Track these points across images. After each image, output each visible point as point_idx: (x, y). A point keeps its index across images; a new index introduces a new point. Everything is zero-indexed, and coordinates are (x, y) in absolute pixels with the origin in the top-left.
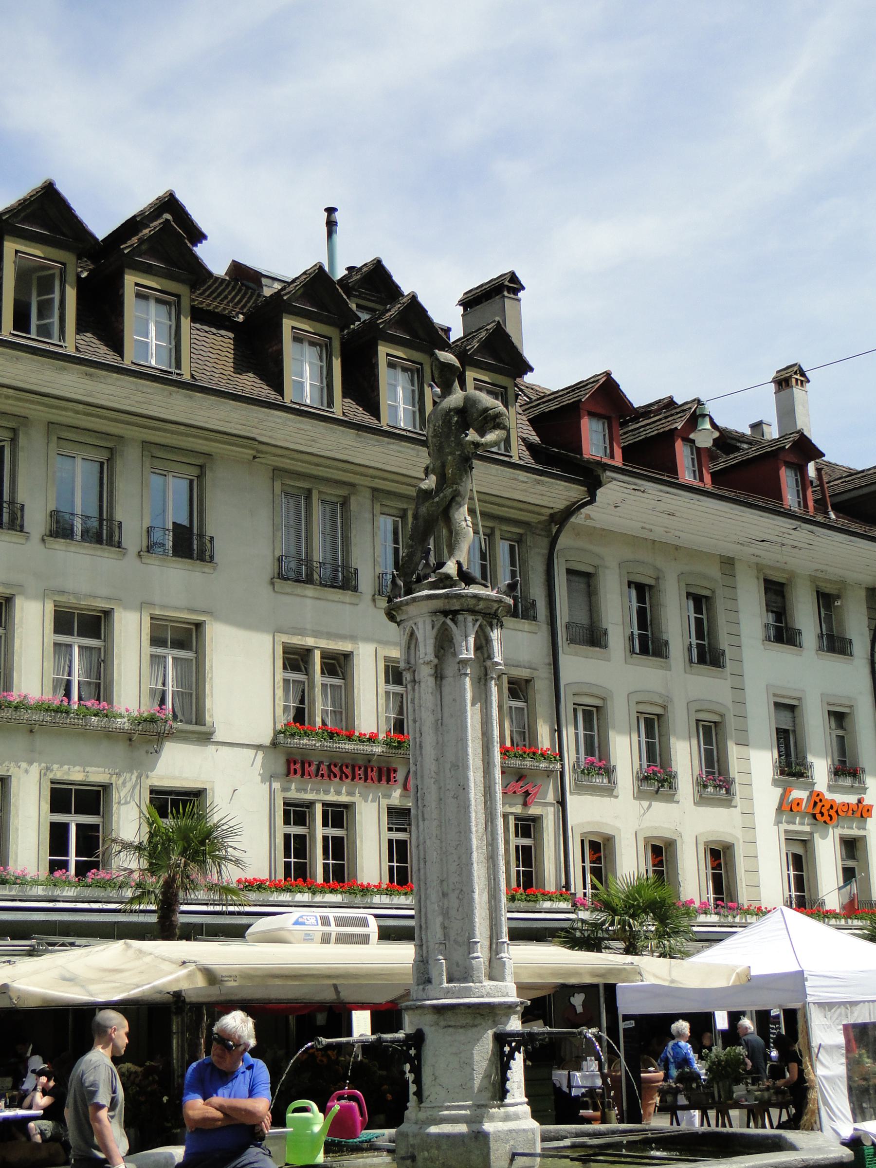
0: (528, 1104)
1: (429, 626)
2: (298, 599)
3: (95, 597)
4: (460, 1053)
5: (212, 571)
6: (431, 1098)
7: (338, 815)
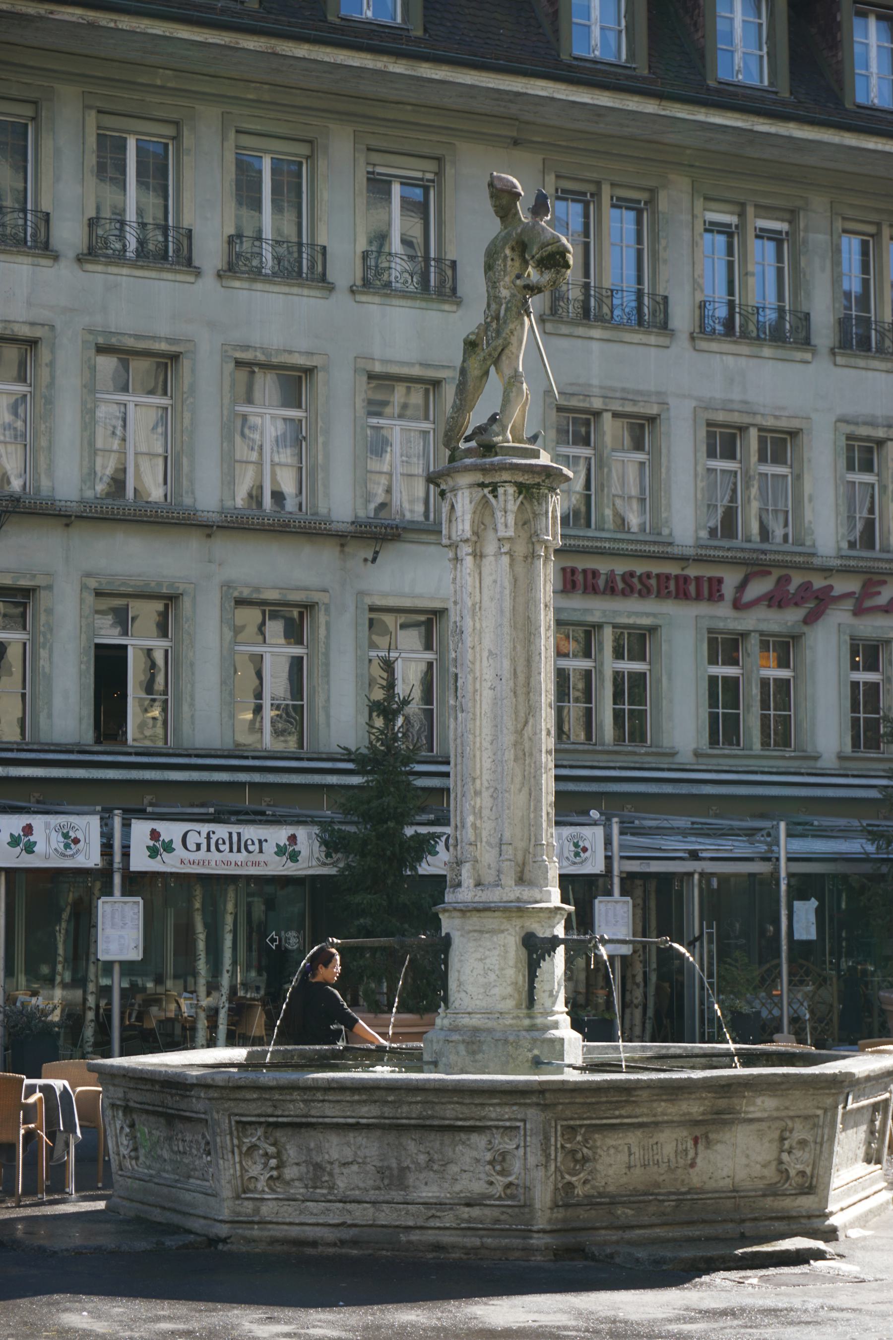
0: (568, 1013)
1: (467, 501)
2: (579, 342)
3: (291, 352)
4: (486, 958)
5: (454, 308)
6: (457, 1004)
7: (637, 641)
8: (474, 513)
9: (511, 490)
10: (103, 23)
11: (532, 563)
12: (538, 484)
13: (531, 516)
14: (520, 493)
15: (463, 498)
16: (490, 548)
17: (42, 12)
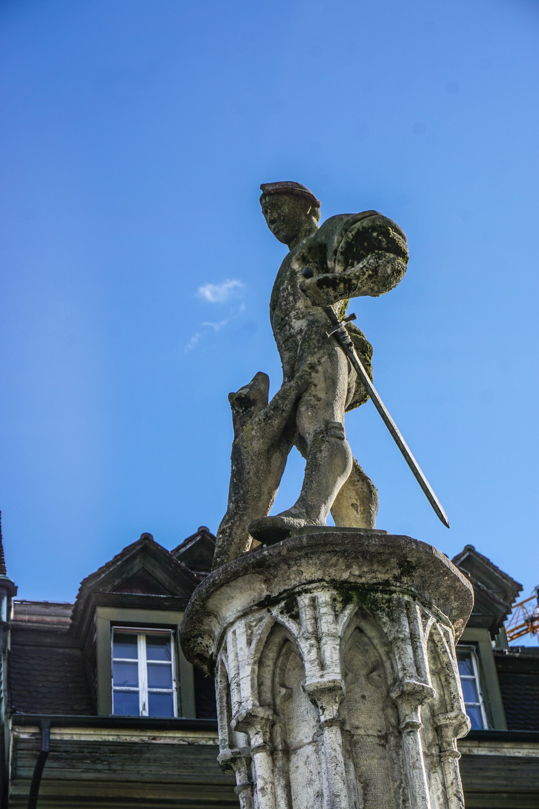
1: (242, 640)
8: (260, 662)
9: (324, 596)
10: (203, 742)
11: (399, 746)
12: (387, 583)
13: (382, 650)
14: (346, 601)
15: (235, 640)
16: (303, 731)
17: (146, 739)
